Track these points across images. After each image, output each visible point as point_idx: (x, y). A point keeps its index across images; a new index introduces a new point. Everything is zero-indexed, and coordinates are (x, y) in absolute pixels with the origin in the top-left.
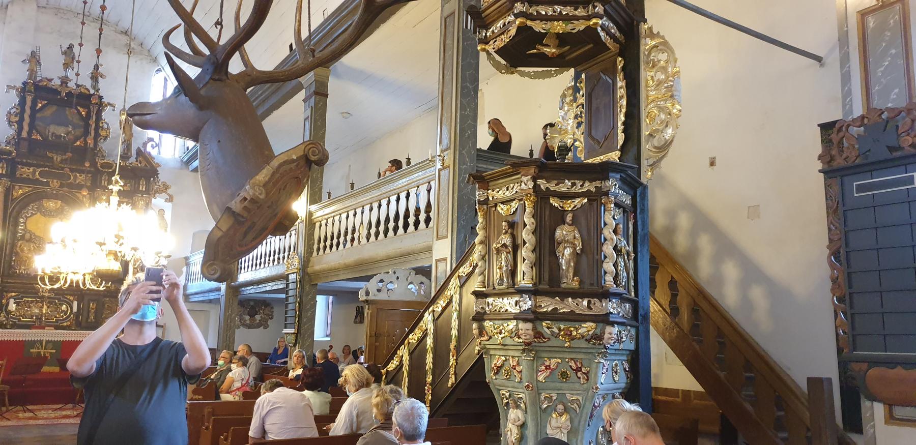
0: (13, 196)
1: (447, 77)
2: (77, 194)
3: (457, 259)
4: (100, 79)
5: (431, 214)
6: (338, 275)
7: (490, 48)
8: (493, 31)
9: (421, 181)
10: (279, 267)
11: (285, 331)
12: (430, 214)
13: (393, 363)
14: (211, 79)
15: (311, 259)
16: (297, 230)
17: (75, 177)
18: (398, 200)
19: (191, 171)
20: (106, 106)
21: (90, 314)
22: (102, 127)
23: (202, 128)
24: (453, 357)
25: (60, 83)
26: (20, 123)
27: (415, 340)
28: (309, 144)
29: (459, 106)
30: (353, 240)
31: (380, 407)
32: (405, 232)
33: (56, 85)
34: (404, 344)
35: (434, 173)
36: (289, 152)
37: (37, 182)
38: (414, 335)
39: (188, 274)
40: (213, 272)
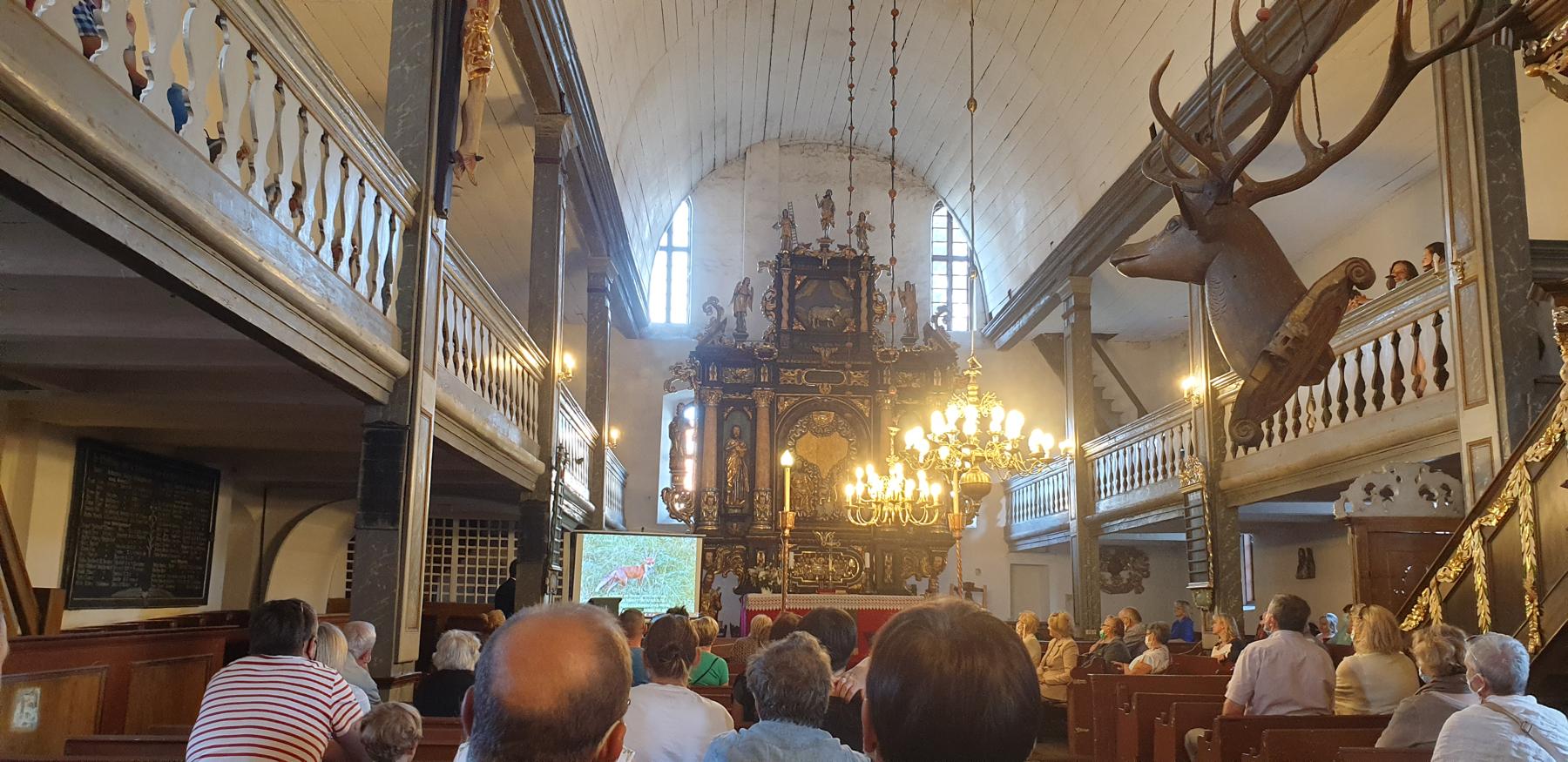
0: (778, 410)
1: (1455, 128)
2: (853, 400)
3: (1513, 441)
4: (868, 232)
5: (1448, 366)
6: (1276, 487)
7: (1550, 68)
8: (1553, 39)
9: (1420, 312)
10: (1166, 483)
11: (1192, 585)
12: (1445, 365)
13: (1412, 619)
14: (1215, 203)
15: (1223, 465)
16: (1192, 422)
17: (849, 376)
18: (1377, 349)
19: (999, 350)
20: (879, 270)
21: (886, 571)
22: (876, 301)
23: (1211, 263)
24: (1532, 601)
25: (819, 248)
26: (778, 311)
27: (1449, 578)
28: (1353, 263)
29: (1485, 172)
30: (1297, 427)
31: (1427, 656)
32: (1343, 421)
33: (815, 251)
34: (1428, 586)
35: (1445, 294)
36: (1329, 276)
37: (804, 389)
38: (1448, 570)
39: (1009, 507)
40: (1245, 433)
